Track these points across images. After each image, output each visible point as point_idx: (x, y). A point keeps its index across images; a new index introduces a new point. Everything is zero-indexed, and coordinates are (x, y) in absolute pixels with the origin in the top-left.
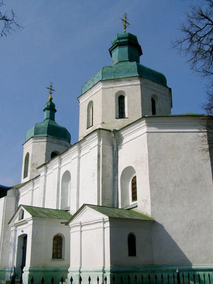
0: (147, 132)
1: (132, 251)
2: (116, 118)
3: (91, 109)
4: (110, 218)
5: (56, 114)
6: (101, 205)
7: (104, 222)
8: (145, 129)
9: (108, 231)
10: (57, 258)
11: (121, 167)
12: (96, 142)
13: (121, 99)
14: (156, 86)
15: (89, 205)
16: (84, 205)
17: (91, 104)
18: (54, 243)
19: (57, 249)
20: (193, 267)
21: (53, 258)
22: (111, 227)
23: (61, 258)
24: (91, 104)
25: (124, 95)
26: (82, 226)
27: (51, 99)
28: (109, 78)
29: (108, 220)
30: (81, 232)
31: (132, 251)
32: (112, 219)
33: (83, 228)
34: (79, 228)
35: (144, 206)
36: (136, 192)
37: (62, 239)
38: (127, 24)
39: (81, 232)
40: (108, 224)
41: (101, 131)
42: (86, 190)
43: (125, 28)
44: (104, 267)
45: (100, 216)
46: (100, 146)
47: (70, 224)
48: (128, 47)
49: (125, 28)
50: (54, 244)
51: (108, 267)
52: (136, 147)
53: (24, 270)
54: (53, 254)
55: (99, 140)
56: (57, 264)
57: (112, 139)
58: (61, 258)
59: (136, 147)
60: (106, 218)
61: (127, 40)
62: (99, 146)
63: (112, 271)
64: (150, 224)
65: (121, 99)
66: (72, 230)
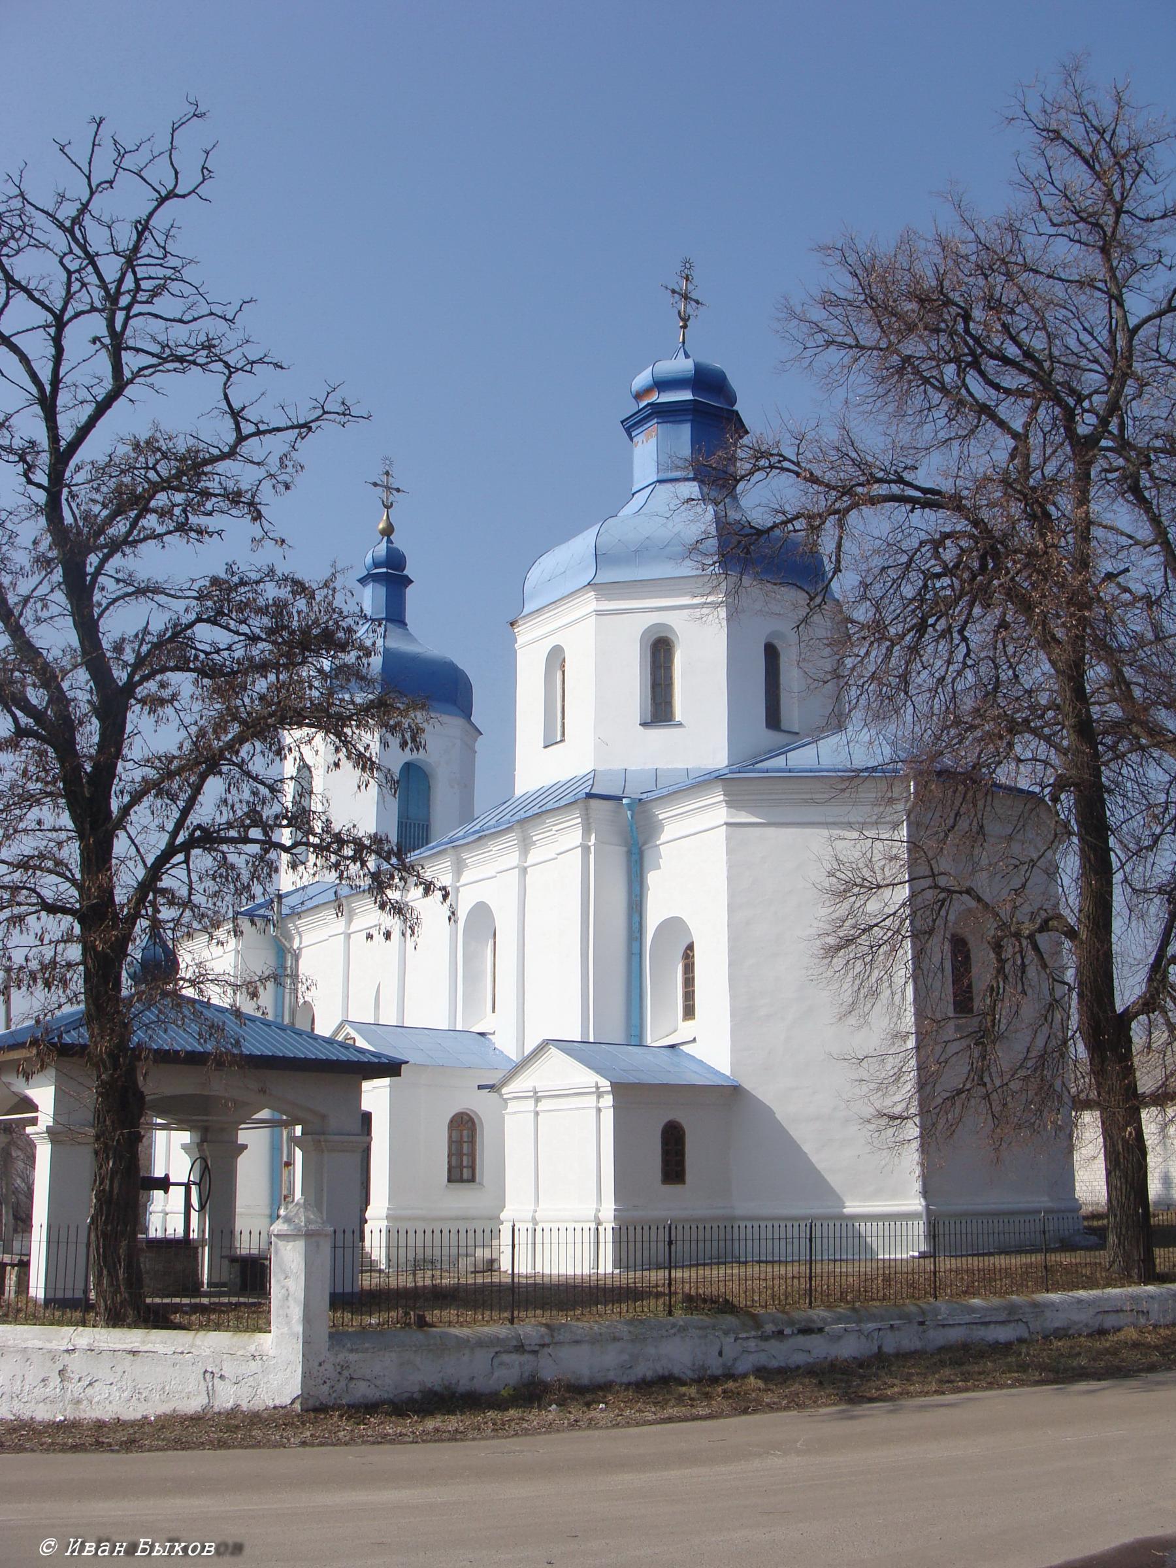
0: (726, 824)
1: (673, 1169)
2: (644, 724)
3: (559, 674)
4: (613, 1085)
5: (409, 590)
6: (592, 1040)
8: (721, 814)
9: (608, 1117)
10: (462, 1181)
11: (653, 920)
13: (660, 651)
16: (545, 1044)
17: (556, 660)
18: (450, 1137)
19: (460, 1154)
20: (845, 1210)
21: (449, 1181)
23: (472, 1180)
24: (556, 660)
25: (673, 638)
26: (538, 1100)
27: (388, 532)
29: (609, 1089)
30: (537, 1114)
31: (673, 1169)
32: (621, 1091)
33: (544, 1105)
34: (530, 1104)
36: (693, 1005)
37: (471, 1120)
38: (691, 309)
40: (608, 1101)
41: (594, 803)
42: (545, 988)
43: (685, 327)
44: (598, 1210)
45: (588, 1078)
46: (589, 847)
47: (504, 1091)
48: (692, 421)
49: (685, 327)
50: (451, 1141)
51: (608, 1209)
52: (696, 866)
53: (368, 1215)
55: (587, 832)
57: (625, 820)
58: (472, 1180)
59: (696, 866)
60: (605, 1084)
62: (586, 849)
64: (729, 1097)
65: (660, 651)
66: (512, 1106)
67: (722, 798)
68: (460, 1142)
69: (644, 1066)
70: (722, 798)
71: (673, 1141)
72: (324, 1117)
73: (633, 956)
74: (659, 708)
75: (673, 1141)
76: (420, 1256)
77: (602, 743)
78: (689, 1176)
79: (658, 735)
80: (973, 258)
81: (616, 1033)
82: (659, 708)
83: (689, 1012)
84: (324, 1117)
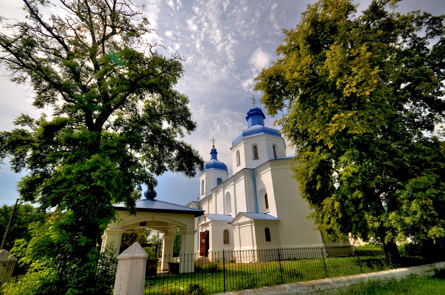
1: (268, 239)
4: (254, 220)
9: (254, 227)
19: (226, 238)
23: (228, 243)
31: (268, 239)
56: (226, 248)
65: (255, 148)
67: (265, 138)
68: (226, 236)
69: (260, 216)
70: (265, 138)
71: (267, 231)
72: (185, 226)
73: (255, 194)
74: (256, 157)
75: (267, 231)
76: (237, 270)
77: (246, 164)
78: (271, 240)
79: (256, 161)
80: (301, 31)
81: (253, 210)
82: (256, 157)
83: (267, 207)
84: (185, 226)
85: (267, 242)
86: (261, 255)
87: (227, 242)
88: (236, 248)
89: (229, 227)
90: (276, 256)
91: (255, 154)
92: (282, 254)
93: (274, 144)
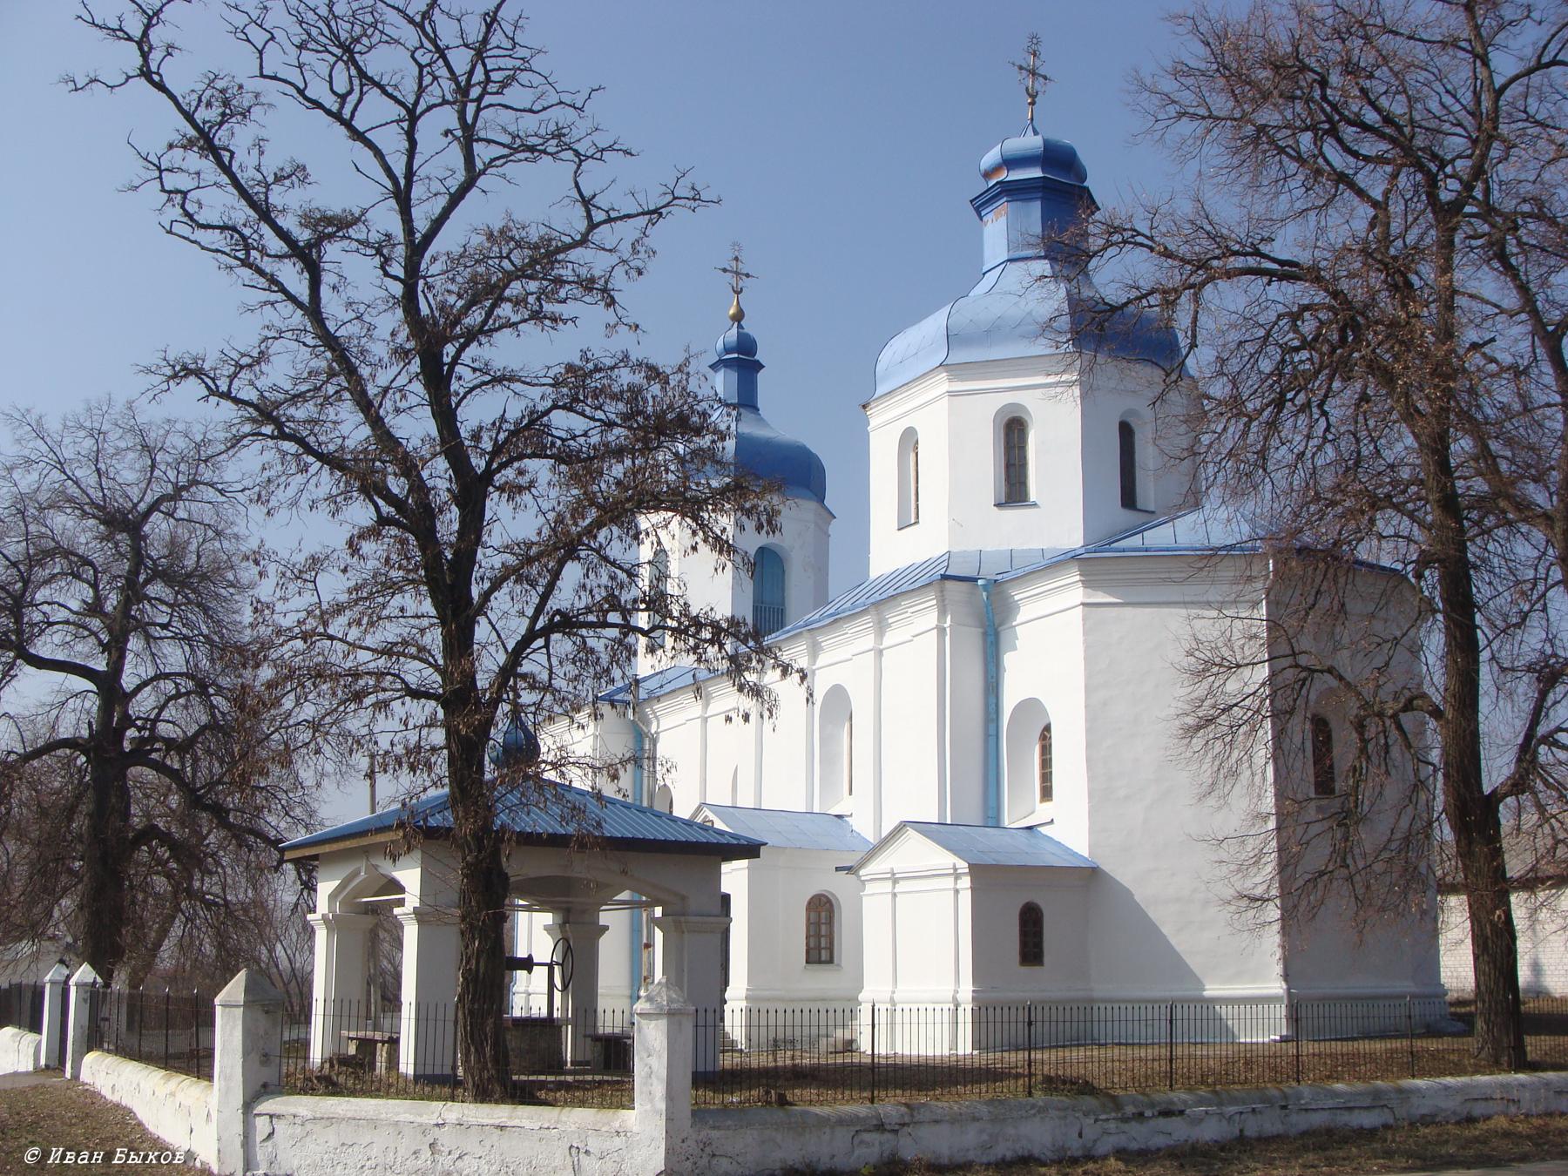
0: (1083, 604)
1: (1032, 951)
2: (998, 505)
4: (971, 866)
5: (761, 376)
7: (957, 876)
8: (1077, 594)
9: (966, 898)
10: (820, 962)
12: (932, 618)
13: (1014, 431)
14: (1146, 377)
15: (916, 825)
16: (903, 826)
17: (909, 442)
18: (808, 919)
19: (819, 936)
22: (974, 889)
23: (831, 961)
24: (909, 442)
26: (895, 881)
27: (738, 317)
28: (966, 353)
30: (895, 895)
31: (1032, 951)
32: (977, 871)
33: (900, 887)
34: (888, 886)
35: (1067, 824)
37: (829, 901)
39: (895, 895)
40: (966, 882)
41: (949, 584)
47: (862, 872)
48: (1043, 199)
50: (809, 923)
51: (966, 990)
52: (1051, 646)
53: (727, 996)
54: (808, 952)
55: (942, 613)
56: (820, 982)
57: (980, 603)
58: (831, 961)
59: (1051, 646)
60: (963, 866)
61: (1036, 173)
62: (941, 631)
63: (211, 1024)
64: (1087, 879)
65: (1014, 431)
68: (818, 924)
69: (1002, 848)
71: (1031, 920)
73: (990, 737)
75: (1031, 920)
79: (1013, 515)
81: (973, 814)
83: (1047, 793)
84: (683, 898)
85: (1026, 970)
86: (702, 1023)
87: (824, 955)
88: (874, 989)
89: (837, 886)
90: (1020, 1026)
91: (1008, 466)
92: (1039, 1018)
93: (1132, 412)
